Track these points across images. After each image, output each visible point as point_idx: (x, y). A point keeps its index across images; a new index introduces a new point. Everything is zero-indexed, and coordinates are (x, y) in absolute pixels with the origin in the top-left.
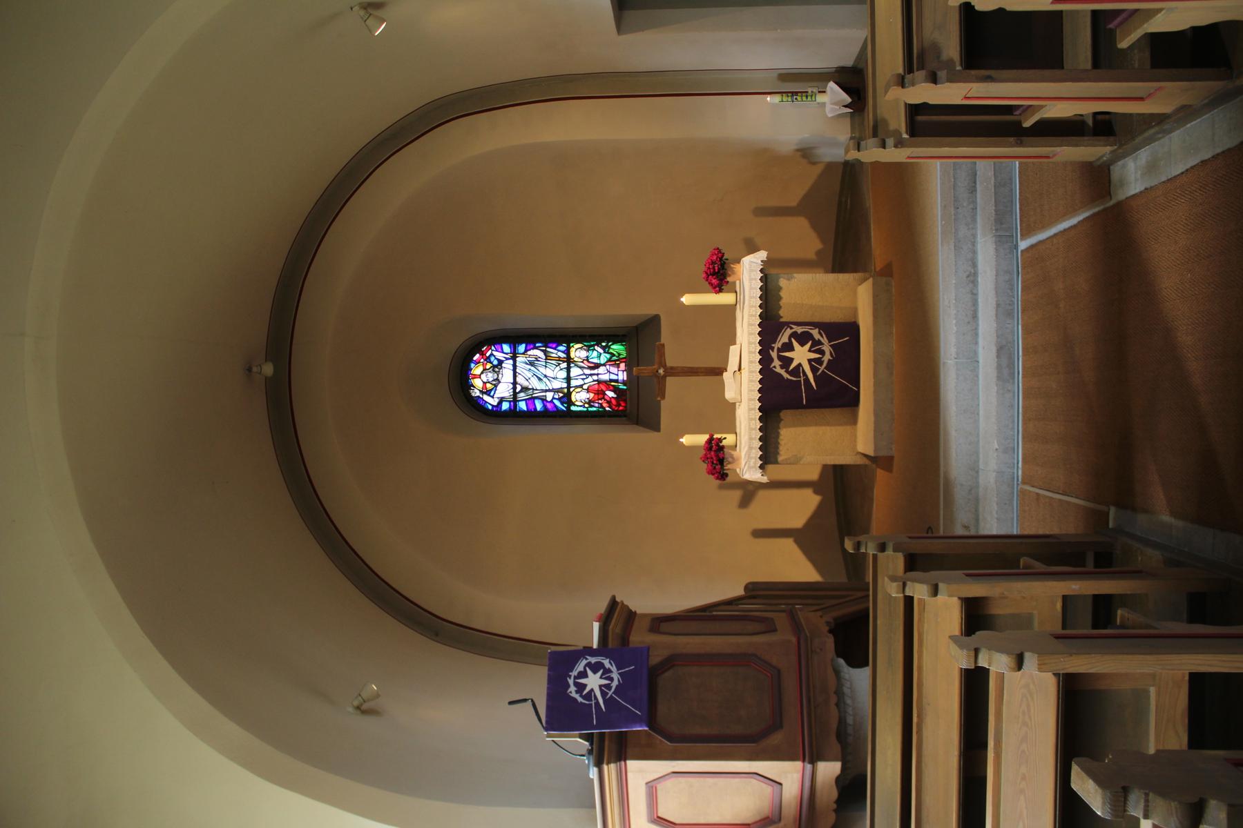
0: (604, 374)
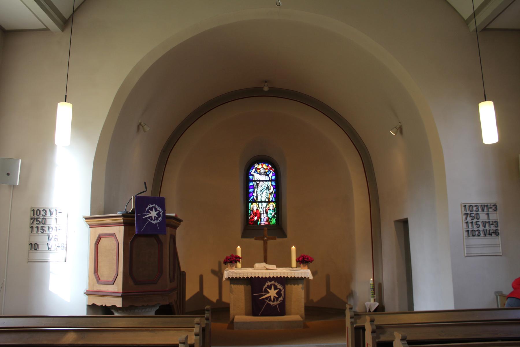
0: (264, 216)
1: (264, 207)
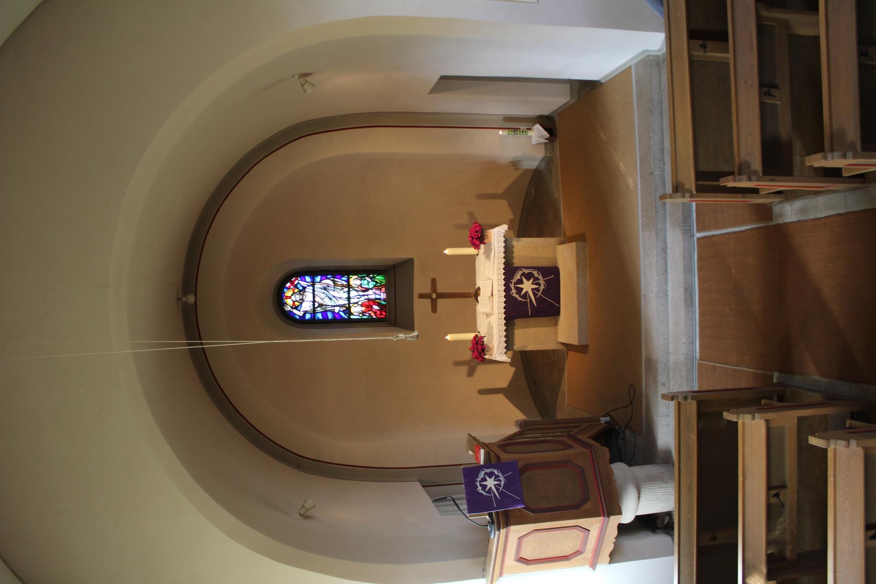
1: (358, 294)
